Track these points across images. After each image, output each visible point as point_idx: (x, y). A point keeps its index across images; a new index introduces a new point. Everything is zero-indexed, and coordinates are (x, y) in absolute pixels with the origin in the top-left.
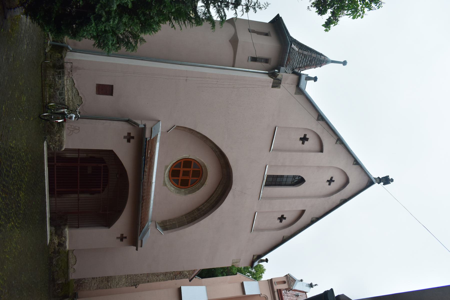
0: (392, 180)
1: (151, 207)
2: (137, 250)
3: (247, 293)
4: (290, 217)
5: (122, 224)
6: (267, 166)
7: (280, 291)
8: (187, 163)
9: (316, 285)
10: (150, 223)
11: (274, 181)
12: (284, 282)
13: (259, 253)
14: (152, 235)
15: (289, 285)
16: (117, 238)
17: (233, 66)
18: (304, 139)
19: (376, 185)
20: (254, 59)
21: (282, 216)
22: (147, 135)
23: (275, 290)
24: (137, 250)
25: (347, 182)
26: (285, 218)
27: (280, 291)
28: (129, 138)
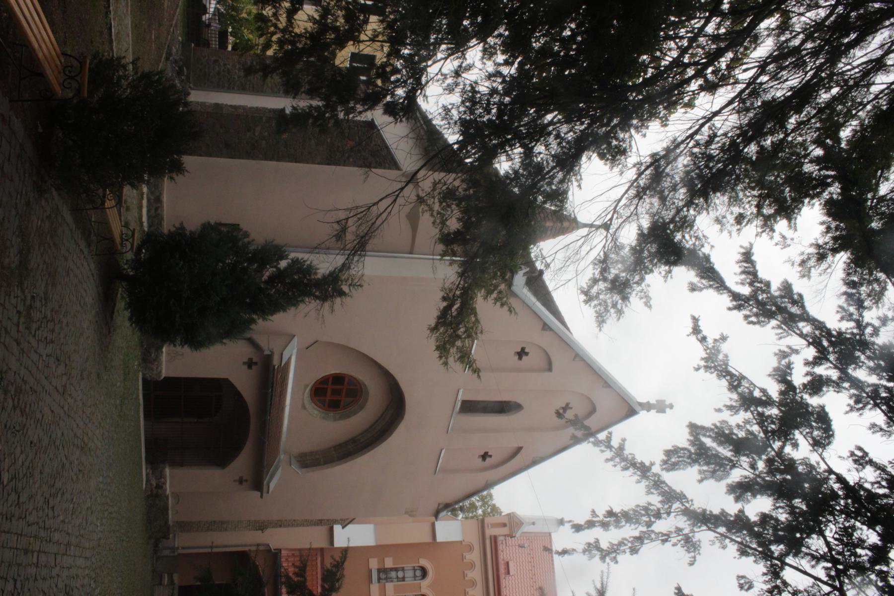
0: (671, 406)
2: (261, 497)
3: (440, 538)
4: (497, 456)
5: (242, 463)
7: (494, 539)
8: (338, 379)
10: (282, 456)
11: (469, 407)
12: (505, 525)
13: (448, 501)
14: (283, 477)
15: (511, 529)
16: (235, 481)
17: (411, 253)
18: (522, 353)
19: (643, 414)
22: (276, 362)
24: (261, 497)
25: (593, 410)
26: (490, 456)
27: (494, 539)
28: (250, 364)
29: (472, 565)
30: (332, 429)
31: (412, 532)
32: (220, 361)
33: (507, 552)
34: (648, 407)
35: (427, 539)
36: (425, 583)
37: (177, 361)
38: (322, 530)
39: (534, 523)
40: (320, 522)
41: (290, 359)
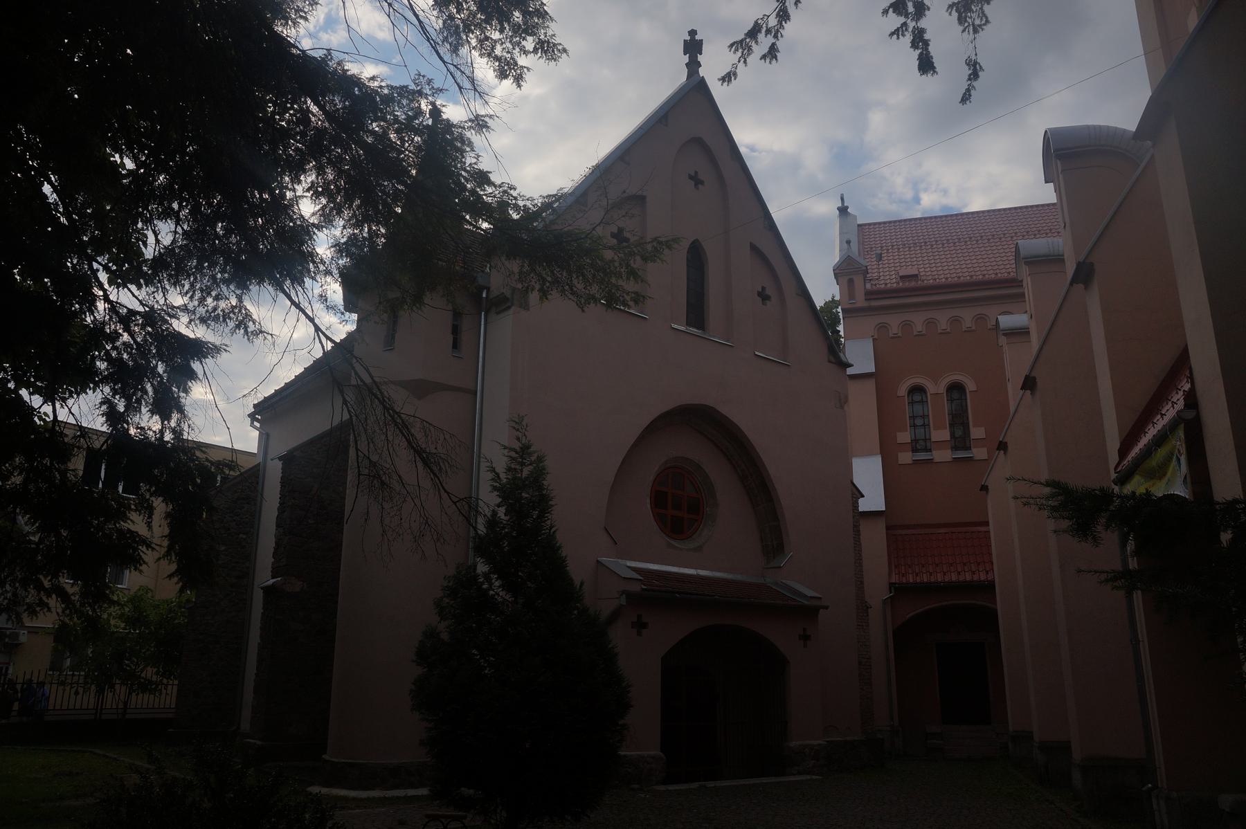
0: (693, 33)
1: (739, 577)
2: (827, 608)
3: (871, 368)
6: (676, 326)
7: (870, 295)
8: (659, 500)
9: (842, 199)
11: (696, 314)
12: (851, 281)
20: (456, 345)
21: (759, 294)
22: (636, 588)
23: (866, 304)
24: (827, 608)
25: (698, 142)
27: (870, 295)
28: (640, 626)
29: (907, 325)
30: (730, 510)
31: (862, 408)
32: (640, 660)
33: (886, 276)
34: (693, 66)
35: (871, 385)
36: (931, 388)
37: (642, 735)
38: (865, 527)
39: (848, 242)
40: (857, 532)
41: (634, 569)
